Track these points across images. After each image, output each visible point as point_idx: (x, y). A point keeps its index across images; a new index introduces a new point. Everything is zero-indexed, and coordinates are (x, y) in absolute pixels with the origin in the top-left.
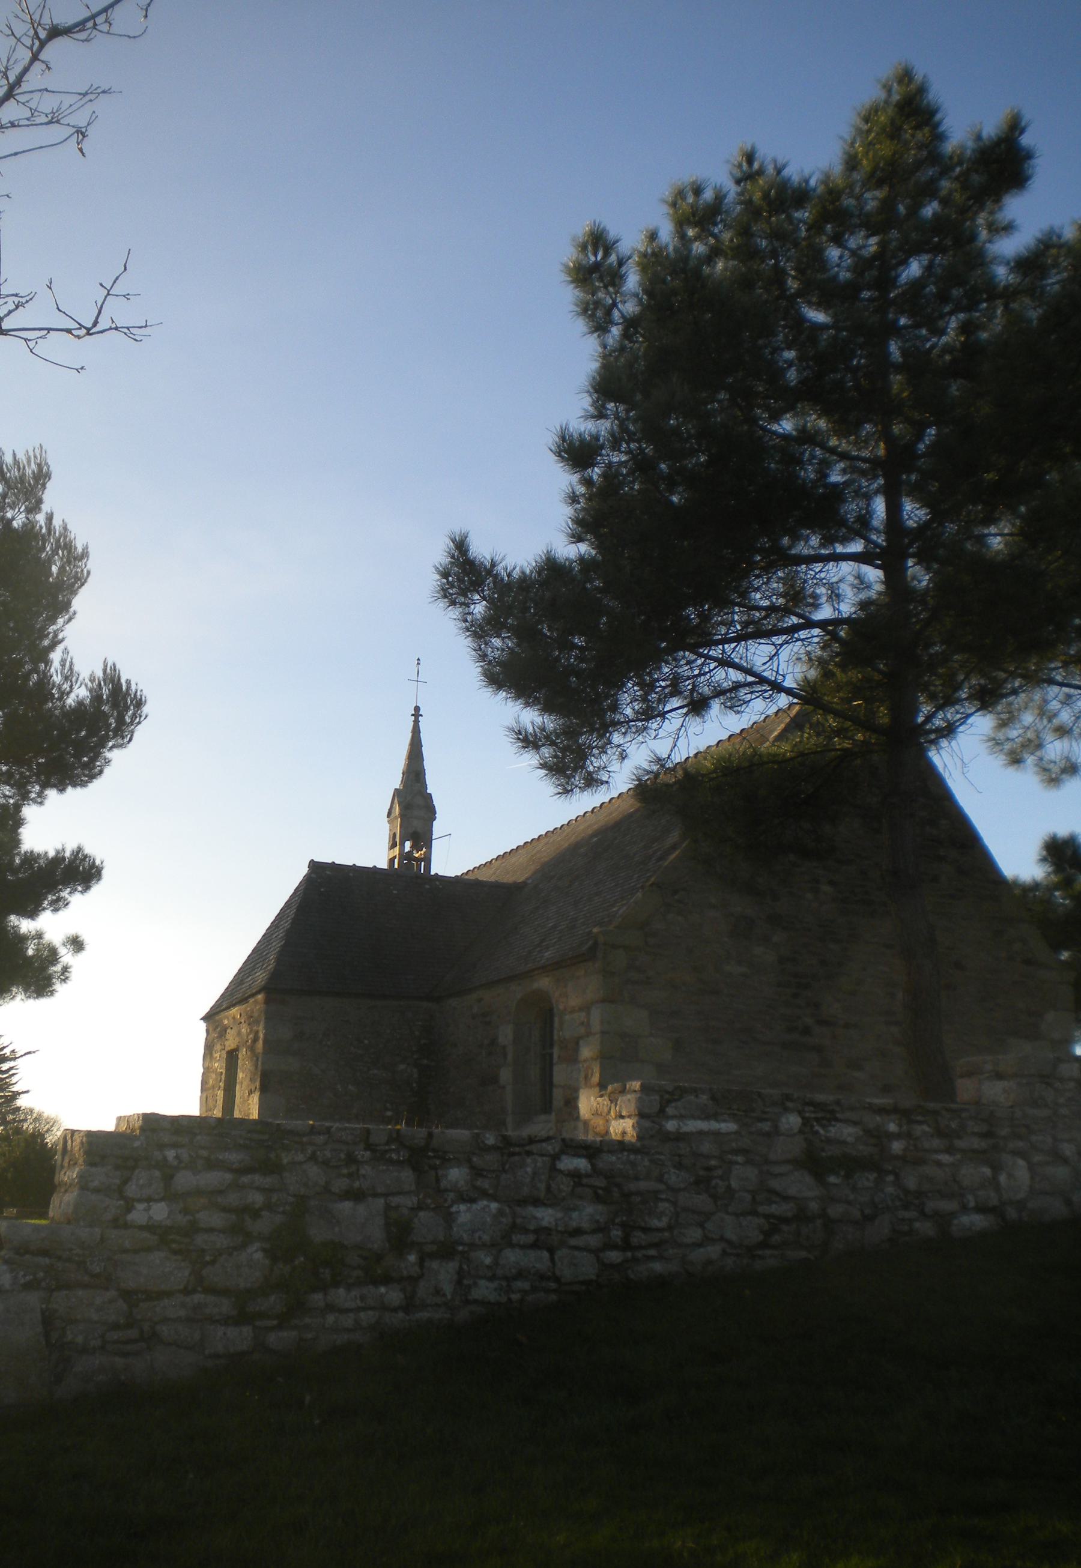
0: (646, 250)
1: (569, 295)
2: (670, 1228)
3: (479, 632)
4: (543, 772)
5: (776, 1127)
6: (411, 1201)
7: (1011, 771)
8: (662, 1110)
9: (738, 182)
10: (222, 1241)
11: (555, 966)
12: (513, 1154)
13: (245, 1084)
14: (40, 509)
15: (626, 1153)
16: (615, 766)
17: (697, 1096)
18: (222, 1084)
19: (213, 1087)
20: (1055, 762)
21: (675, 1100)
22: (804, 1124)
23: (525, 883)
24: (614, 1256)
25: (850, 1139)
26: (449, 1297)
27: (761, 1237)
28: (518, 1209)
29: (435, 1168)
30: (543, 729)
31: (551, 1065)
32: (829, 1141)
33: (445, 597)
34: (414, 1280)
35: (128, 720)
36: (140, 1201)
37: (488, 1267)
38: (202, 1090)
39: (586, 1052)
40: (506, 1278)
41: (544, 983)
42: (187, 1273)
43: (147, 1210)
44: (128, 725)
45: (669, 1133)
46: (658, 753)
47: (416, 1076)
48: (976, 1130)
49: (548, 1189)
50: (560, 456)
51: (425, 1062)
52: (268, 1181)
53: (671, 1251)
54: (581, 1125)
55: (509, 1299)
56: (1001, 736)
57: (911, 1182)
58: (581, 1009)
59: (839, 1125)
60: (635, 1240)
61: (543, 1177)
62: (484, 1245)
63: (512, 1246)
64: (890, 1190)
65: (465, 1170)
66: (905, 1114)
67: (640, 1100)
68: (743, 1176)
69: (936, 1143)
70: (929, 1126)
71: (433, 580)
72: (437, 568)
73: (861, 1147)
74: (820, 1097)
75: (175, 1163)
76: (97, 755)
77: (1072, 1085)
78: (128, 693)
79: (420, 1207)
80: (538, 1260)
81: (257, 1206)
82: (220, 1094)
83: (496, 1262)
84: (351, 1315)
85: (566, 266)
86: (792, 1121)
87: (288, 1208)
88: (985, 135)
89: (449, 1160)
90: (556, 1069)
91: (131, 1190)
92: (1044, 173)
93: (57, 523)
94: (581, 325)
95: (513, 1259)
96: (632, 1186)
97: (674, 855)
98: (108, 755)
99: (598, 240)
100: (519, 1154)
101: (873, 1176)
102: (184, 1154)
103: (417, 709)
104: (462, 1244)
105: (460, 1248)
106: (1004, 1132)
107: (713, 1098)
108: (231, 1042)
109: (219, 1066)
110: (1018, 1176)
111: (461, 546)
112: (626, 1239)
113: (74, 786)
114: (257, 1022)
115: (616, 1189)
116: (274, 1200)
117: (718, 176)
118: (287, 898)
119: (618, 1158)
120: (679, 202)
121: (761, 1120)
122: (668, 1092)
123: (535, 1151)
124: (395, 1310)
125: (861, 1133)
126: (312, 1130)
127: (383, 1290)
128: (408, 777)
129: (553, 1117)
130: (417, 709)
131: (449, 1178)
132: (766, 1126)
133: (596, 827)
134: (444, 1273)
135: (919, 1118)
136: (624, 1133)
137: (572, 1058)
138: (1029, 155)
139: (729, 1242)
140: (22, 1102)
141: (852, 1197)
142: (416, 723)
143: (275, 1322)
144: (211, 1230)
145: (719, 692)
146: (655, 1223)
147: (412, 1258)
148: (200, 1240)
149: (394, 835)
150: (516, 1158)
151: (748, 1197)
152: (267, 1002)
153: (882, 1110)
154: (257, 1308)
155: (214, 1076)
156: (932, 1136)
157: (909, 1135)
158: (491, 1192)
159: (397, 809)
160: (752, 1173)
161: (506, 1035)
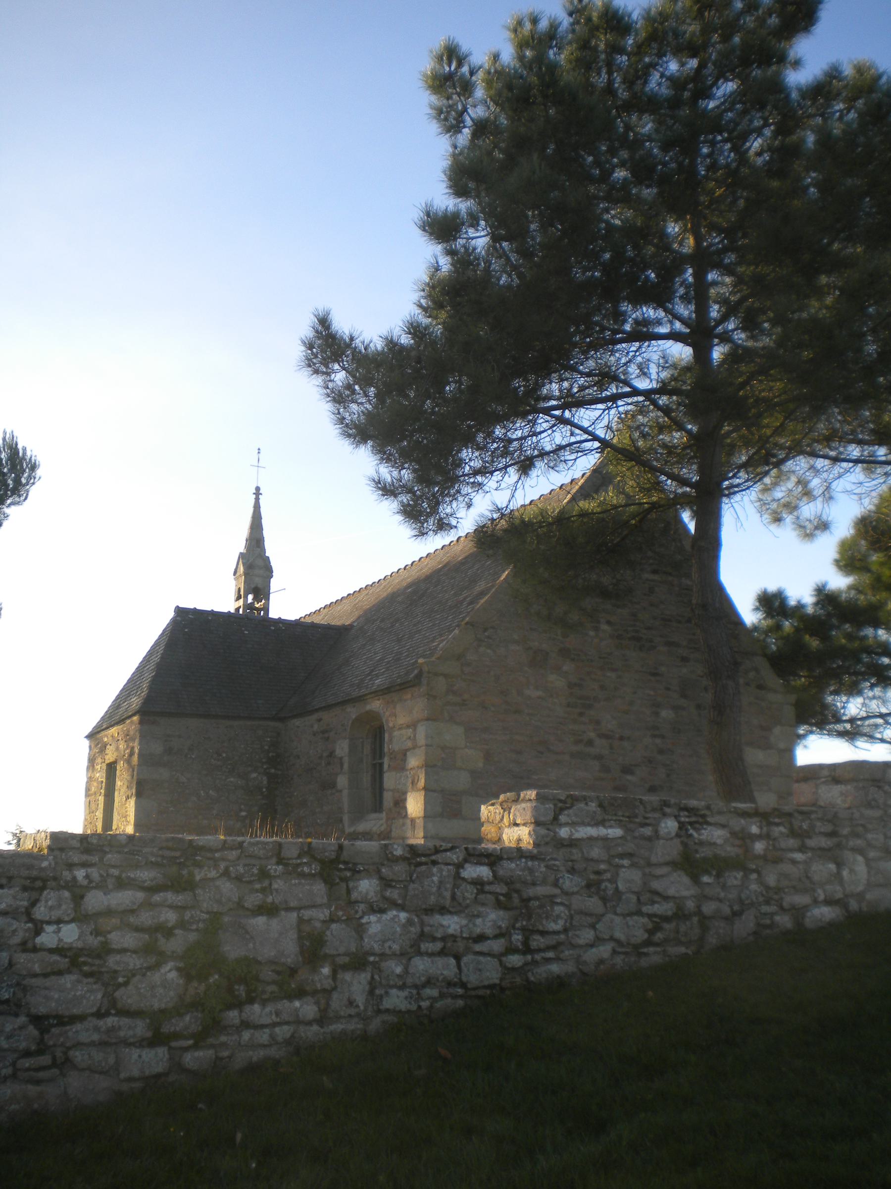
0: (490, 69)
1: (424, 100)
2: (565, 930)
3: (339, 398)
6: (322, 914)
7: (773, 527)
8: (556, 818)
9: (570, 14)
10: (134, 962)
12: (420, 864)
15: (524, 860)
16: (461, 513)
17: (586, 804)
18: (103, 791)
20: (810, 521)
22: (680, 828)
24: (515, 960)
25: (719, 841)
26: (362, 1008)
27: (646, 936)
28: (425, 918)
29: (345, 880)
32: (701, 843)
33: (309, 366)
34: (327, 992)
35: (24, 481)
36: (49, 923)
37: (399, 976)
39: (414, 761)
40: (416, 986)
41: (376, 705)
42: (99, 996)
43: (59, 931)
44: (24, 485)
47: (265, 782)
48: (822, 830)
49: (453, 897)
50: (424, 230)
51: (273, 771)
53: (567, 953)
54: (408, 822)
55: (420, 1007)
56: (767, 497)
57: (771, 880)
58: (408, 727)
59: (709, 828)
60: (535, 943)
61: (448, 886)
62: (394, 954)
63: (420, 953)
64: (754, 887)
65: (375, 881)
67: (535, 809)
68: (629, 878)
69: (792, 842)
70: (785, 828)
71: (299, 351)
72: (304, 343)
73: (728, 849)
74: (693, 803)
75: (85, 882)
78: (24, 458)
79: (332, 920)
80: (445, 967)
81: (170, 925)
82: (101, 799)
83: (406, 971)
84: (267, 1030)
85: (425, 75)
86: (670, 825)
87: (201, 925)
89: (359, 872)
91: (40, 912)
94: (434, 127)
95: (421, 967)
96: (531, 892)
97: (482, 601)
98: (7, 510)
100: (426, 864)
101: (740, 875)
102: (95, 873)
103: (258, 489)
104: (374, 954)
105: (372, 959)
106: (845, 831)
107: (601, 805)
108: (110, 757)
109: (100, 775)
110: (858, 873)
111: (324, 321)
112: (526, 943)
114: (133, 740)
115: (515, 895)
118: (156, 637)
119: (517, 865)
122: (561, 801)
124: (309, 1023)
125: (728, 835)
126: (224, 846)
127: (297, 1004)
129: (384, 815)
130: (258, 489)
131: (360, 889)
132: (647, 831)
134: (357, 985)
135: (777, 820)
136: (519, 840)
137: (400, 765)
139: (618, 941)
141: (722, 895)
142: (257, 500)
143: (191, 1042)
144: (124, 951)
146: (553, 926)
147: (326, 971)
149: (239, 589)
150: (423, 868)
151: (634, 898)
152: (141, 722)
153: (745, 814)
154: (172, 1029)
155: (95, 784)
156: (788, 836)
157: (768, 836)
158: (400, 902)
160: (635, 876)
161: (342, 748)
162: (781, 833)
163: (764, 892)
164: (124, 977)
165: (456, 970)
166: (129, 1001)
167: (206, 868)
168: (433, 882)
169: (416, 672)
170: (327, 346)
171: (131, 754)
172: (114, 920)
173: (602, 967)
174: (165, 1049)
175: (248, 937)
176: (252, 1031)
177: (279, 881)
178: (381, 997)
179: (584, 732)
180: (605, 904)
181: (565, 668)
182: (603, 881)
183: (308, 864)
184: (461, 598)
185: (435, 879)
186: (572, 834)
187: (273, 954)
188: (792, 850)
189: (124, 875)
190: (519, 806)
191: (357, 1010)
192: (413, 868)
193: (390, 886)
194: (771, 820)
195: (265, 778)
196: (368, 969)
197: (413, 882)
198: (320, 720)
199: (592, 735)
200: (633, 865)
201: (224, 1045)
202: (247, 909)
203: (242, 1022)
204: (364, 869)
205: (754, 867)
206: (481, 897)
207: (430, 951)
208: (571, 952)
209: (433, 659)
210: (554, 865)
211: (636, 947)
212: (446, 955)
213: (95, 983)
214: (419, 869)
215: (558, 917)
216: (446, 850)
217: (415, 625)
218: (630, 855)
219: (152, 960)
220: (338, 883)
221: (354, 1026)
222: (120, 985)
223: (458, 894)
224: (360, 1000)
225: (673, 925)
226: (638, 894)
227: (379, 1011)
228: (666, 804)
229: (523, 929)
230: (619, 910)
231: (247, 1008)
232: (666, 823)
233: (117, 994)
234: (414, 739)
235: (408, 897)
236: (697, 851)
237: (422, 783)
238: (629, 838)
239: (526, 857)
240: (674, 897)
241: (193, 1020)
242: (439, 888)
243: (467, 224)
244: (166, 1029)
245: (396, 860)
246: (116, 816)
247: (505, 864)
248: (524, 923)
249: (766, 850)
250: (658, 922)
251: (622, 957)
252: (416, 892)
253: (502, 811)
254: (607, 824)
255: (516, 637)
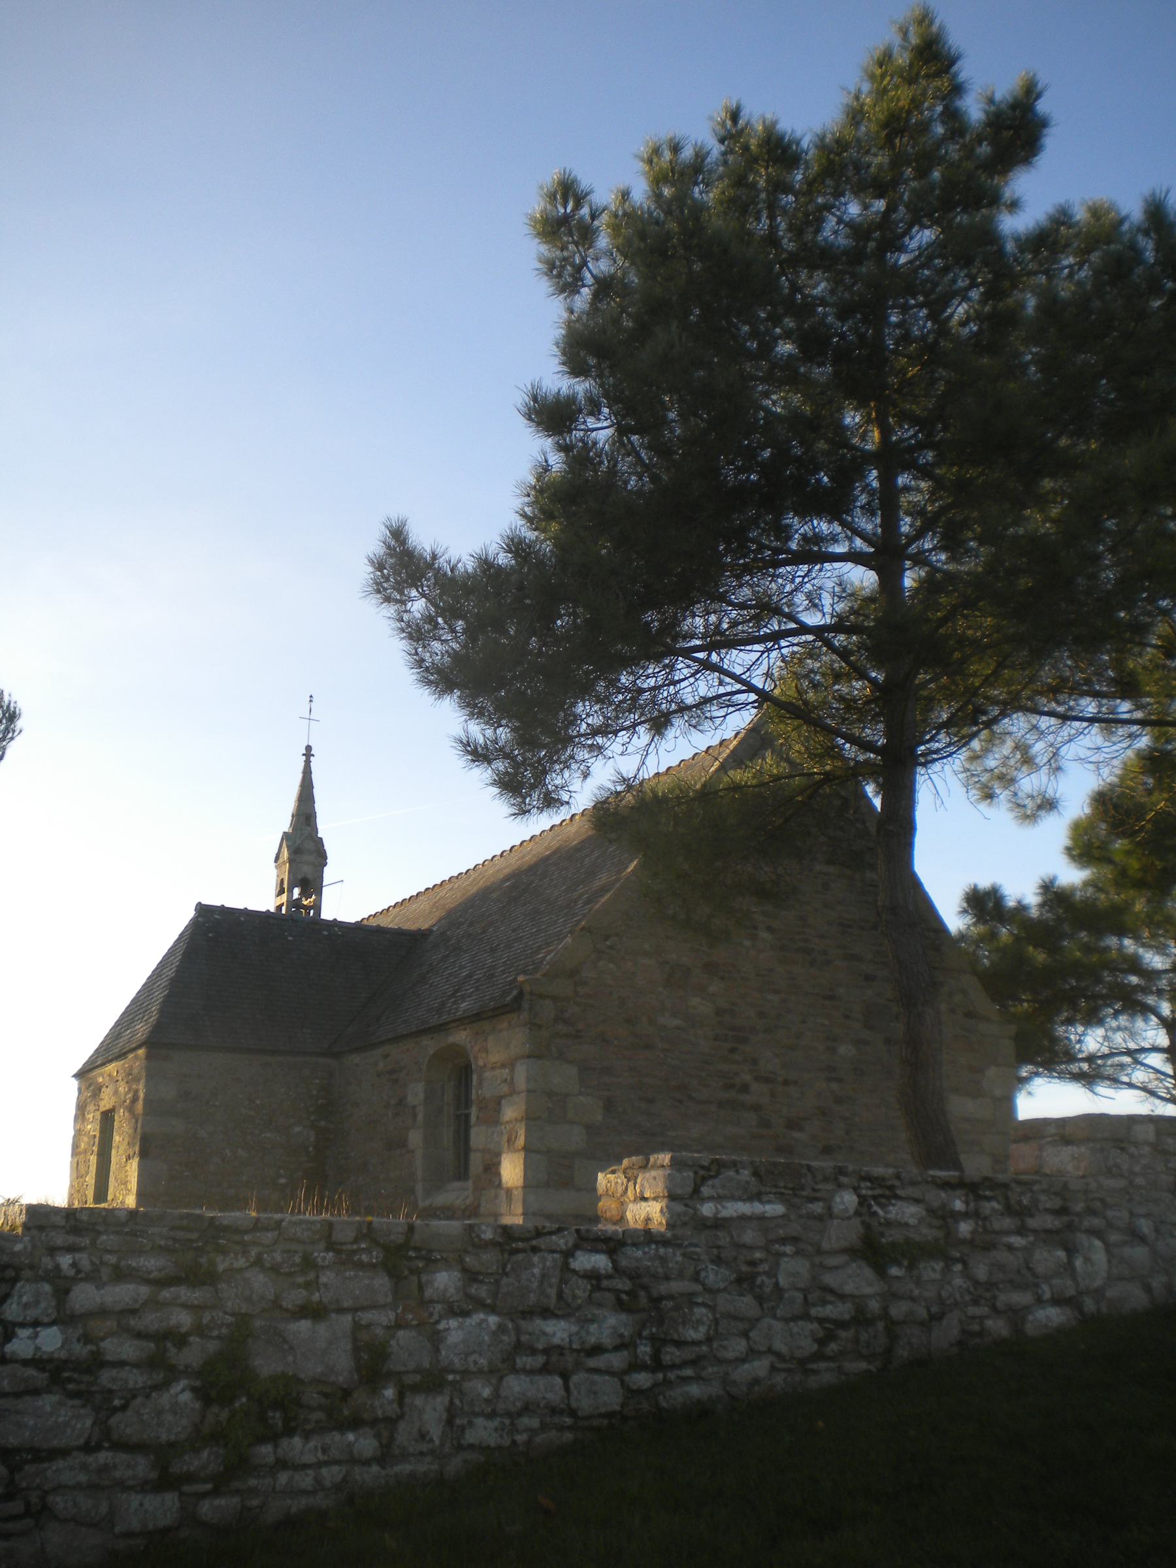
1: (531, 251)
2: (709, 1340)
3: (417, 634)
4: (496, 790)
5: (829, 1208)
6: (386, 1317)
7: (983, 806)
8: (696, 1191)
9: (722, 141)
11: (476, 1017)
12: (517, 1251)
13: (122, 1149)
17: (737, 1172)
18: (95, 1149)
19: (85, 1151)
21: (711, 1177)
22: (860, 1204)
24: (642, 1379)
25: (912, 1221)
26: (437, 1442)
28: (523, 1324)
30: (495, 741)
32: (889, 1224)
33: (378, 592)
34: (392, 1422)
36: (23, 1325)
37: (487, 1401)
39: (510, 1113)
40: (509, 1414)
41: (461, 1037)
42: (89, 1423)
43: (36, 1335)
45: (706, 1218)
47: (312, 1139)
49: (560, 1296)
50: (530, 419)
51: (323, 1123)
52: (196, 1295)
53: (710, 1370)
54: (503, 1193)
55: (514, 1442)
57: (981, 1272)
58: (503, 1066)
59: (899, 1203)
60: (668, 1358)
61: (553, 1280)
63: (515, 1371)
64: (958, 1281)
65: (456, 1274)
67: (670, 1178)
68: (793, 1270)
69: (1008, 1222)
70: (998, 1202)
73: (925, 1231)
74: (879, 1171)
75: (72, 1273)
77: (1146, 1150)
79: (399, 1325)
80: (549, 1389)
81: (183, 1330)
82: (93, 1159)
84: (310, 1472)
86: (847, 1200)
88: (998, 97)
89: (436, 1261)
90: (473, 1132)
92: (1055, 146)
94: (544, 286)
95: (517, 1389)
96: (663, 1288)
99: (567, 190)
100: (524, 1251)
101: (939, 1266)
102: (84, 1259)
103: (309, 748)
105: (450, 1377)
107: (756, 1174)
109: (92, 1127)
110: (1095, 1260)
111: (398, 534)
112: (656, 1356)
114: (137, 1080)
115: (642, 1294)
116: (205, 1321)
117: (700, 133)
119: (645, 1253)
120: (655, 160)
122: (703, 1167)
124: (367, 1463)
125: (924, 1213)
126: (257, 1226)
127: (351, 1437)
128: (298, 820)
129: (470, 1183)
130: (309, 748)
131: (436, 1284)
132: (818, 1208)
133: (507, 871)
134: (430, 1412)
136: (648, 1219)
138: (1043, 123)
139: (778, 1354)
141: (916, 1292)
142: (308, 764)
143: (209, 1486)
144: (122, 1364)
145: (683, 709)
146: (692, 1334)
147: (389, 1393)
148: (106, 1377)
150: (520, 1256)
151: (799, 1296)
152: (148, 1057)
153: (946, 1185)
154: (185, 1468)
155: (86, 1139)
157: (976, 1215)
158: (489, 1301)
159: (285, 854)
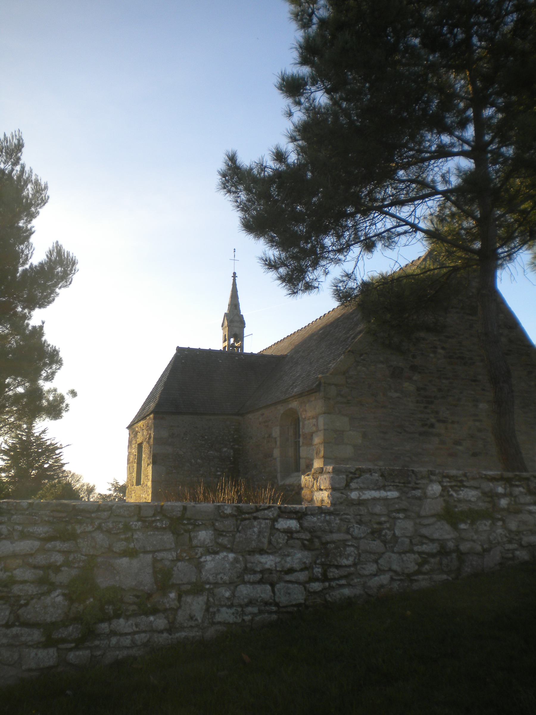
2: (355, 565)
5: (425, 493)
8: (347, 485)
10: (32, 589)
11: (300, 395)
12: (245, 519)
14: (18, 163)
15: (323, 515)
16: (322, 278)
17: (371, 475)
18: (136, 460)
22: (442, 490)
23: (286, 355)
24: (316, 586)
25: (473, 499)
26: (200, 621)
27: (417, 567)
30: (280, 259)
31: (299, 447)
32: (460, 501)
33: (224, 188)
34: (175, 610)
37: (228, 599)
38: (128, 464)
39: (317, 440)
40: (241, 606)
41: (294, 404)
42: (7, 613)
45: (353, 500)
46: (347, 271)
47: (232, 454)
49: (270, 542)
50: (281, 90)
51: (236, 446)
52: (65, 546)
53: (356, 581)
55: (243, 620)
57: (513, 526)
58: (313, 418)
59: (466, 490)
60: (331, 574)
61: (266, 534)
62: (225, 583)
63: (244, 583)
64: (500, 531)
65: (211, 532)
66: (508, 481)
67: (332, 479)
68: (404, 527)
69: (528, 499)
70: (524, 488)
71: (217, 179)
72: (219, 172)
73: (480, 504)
74: (453, 472)
76: (53, 291)
79: (179, 559)
80: (264, 592)
81: (58, 564)
82: (135, 465)
83: (233, 595)
86: (435, 489)
93: (27, 169)
95: (245, 592)
96: (328, 538)
101: (489, 523)
103: (234, 274)
104: (209, 583)
105: (207, 586)
107: (382, 475)
108: (139, 440)
109: (135, 451)
113: (40, 307)
114: (150, 429)
119: (318, 519)
121: (414, 489)
122: (351, 473)
123: (260, 517)
124: (161, 632)
125: (480, 495)
127: (152, 618)
130: (234, 274)
131: (199, 538)
132: (418, 493)
133: (321, 326)
134: (196, 605)
135: (517, 483)
136: (322, 501)
137: (310, 443)
139: (395, 572)
140: (65, 468)
141: (475, 537)
142: (234, 280)
143: (73, 645)
144: (24, 582)
146: (345, 562)
147: (173, 595)
149: (225, 335)
150: (247, 522)
151: (407, 541)
152: (155, 418)
153: (493, 479)
154: (60, 636)
155: (132, 456)
156: (526, 494)
157: (511, 495)
158: (229, 546)
160: (409, 525)
161: (276, 432)
162: (521, 492)
163: (507, 535)
164: (25, 600)
165: (271, 594)
166: (28, 617)
167: (85, 525)
168: (254, 532)
169: (317, 383)
170: (235, 176)
171: (150, 438)
172: (18, 561)
173: (382, 590)
174: (55, 649)
175: (115, 572)
176: (119, 637)
177: (138, 533)
178: (214, 613)
179: (428, 419)
180: (385, 545)
181: (415, 378)
182: (384, 529)
183: (161, 521)
184: (348, 335)
185: (256, 530)
186: (360, 496)
187: (134, 584)
188: (530, 504)
189: (26, 530)
190: (322, 477)
191: (196, 622)
192: (239, 522)
193: (221, 535)
194: (513, 483)
195: (232, 451)
196: (204, 593)
197: (240, 532)
198: (263, 414)
199: (433, 420)
200: (407, 517)
201: (97, 647)
202: (116, 552)
203: (111, 631)
204: (203, 524)
205: (500, 517)
206: (291, 542)
207: (251, 580)
208: (359, 580)
209: (328, 375)
210: (346, 518)
211: (409, 575)
212: (264, 583)
213: (4, 604)
214: (243, 523)
215: (349, 555)
216: (265, 509)
217: (321, 354)
218: (404, 510)
219: (45, 588)
220: (183, 534)
221: (194, 633)
222: (21, 606)
223: (273, 540)
224: (199, 616)
225: (438, 559)
226: (411, 538)
227: (213, 623)
228: (432, 473)
229: (322, 564)
230: (396, 549)
231: (114, 622)
232: (432, 487)
233: (20, 612)
234: (316, 425)
235: (235, 543)
236: (456, 506)
237: (322, 454)
238: (403, 498)
239: (325, 513)
240: (438, 540)
241: (75, 630)
242: (259, 536)
243: (309, 83)
244: (56, 635)
245: (226, 517)
246: (143, 476)
247: (309, 518)
248: (323, 560)
249: (509, 504)
250: (425, 558)
251: (398, 583)
252: (241, 539)
253: (313, 480)
254: (387, 488)
255: (382, 359)
